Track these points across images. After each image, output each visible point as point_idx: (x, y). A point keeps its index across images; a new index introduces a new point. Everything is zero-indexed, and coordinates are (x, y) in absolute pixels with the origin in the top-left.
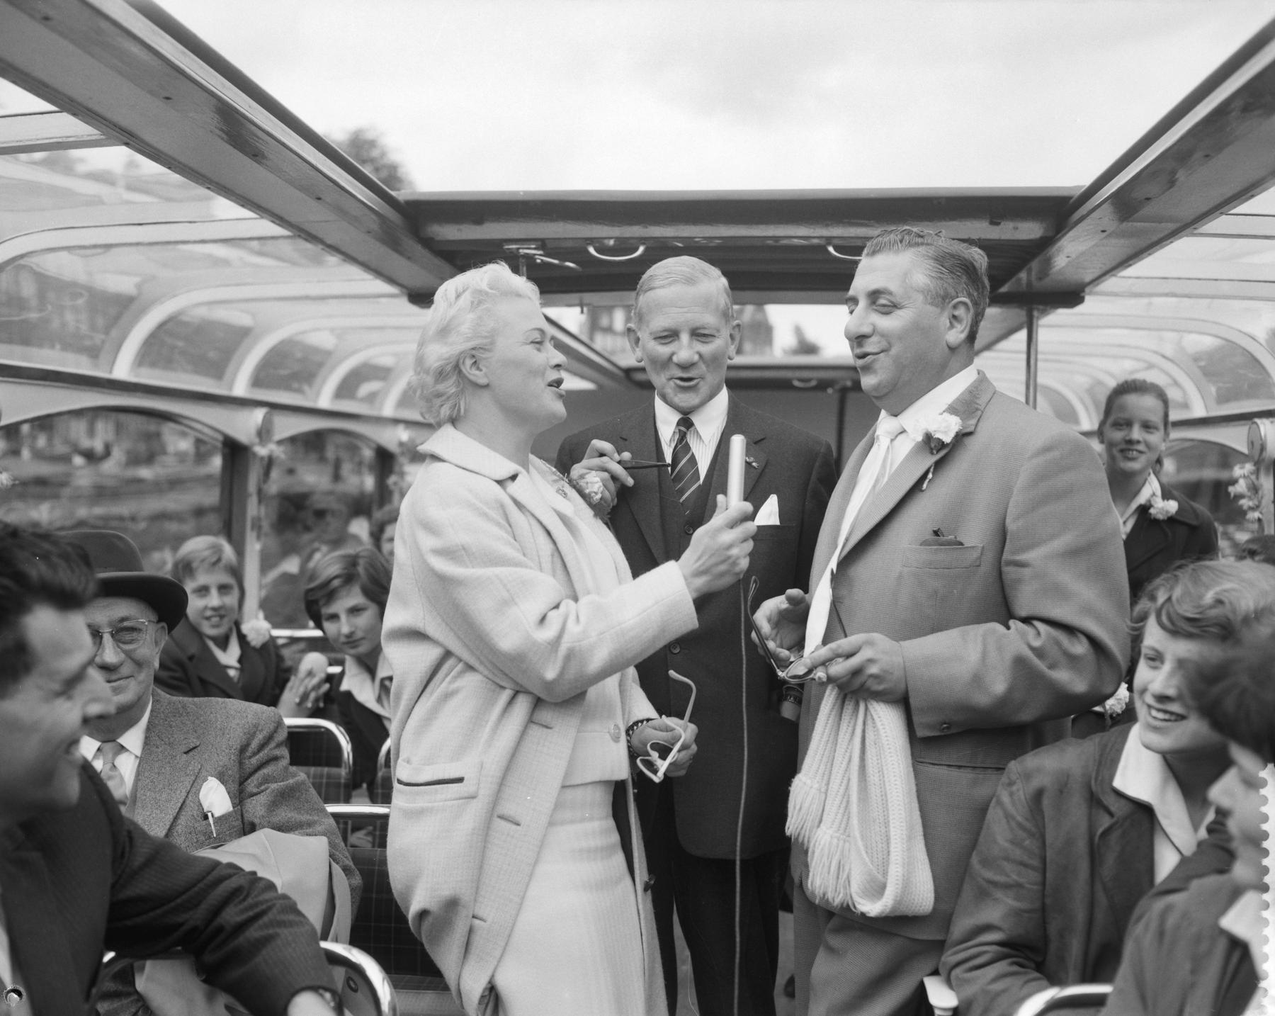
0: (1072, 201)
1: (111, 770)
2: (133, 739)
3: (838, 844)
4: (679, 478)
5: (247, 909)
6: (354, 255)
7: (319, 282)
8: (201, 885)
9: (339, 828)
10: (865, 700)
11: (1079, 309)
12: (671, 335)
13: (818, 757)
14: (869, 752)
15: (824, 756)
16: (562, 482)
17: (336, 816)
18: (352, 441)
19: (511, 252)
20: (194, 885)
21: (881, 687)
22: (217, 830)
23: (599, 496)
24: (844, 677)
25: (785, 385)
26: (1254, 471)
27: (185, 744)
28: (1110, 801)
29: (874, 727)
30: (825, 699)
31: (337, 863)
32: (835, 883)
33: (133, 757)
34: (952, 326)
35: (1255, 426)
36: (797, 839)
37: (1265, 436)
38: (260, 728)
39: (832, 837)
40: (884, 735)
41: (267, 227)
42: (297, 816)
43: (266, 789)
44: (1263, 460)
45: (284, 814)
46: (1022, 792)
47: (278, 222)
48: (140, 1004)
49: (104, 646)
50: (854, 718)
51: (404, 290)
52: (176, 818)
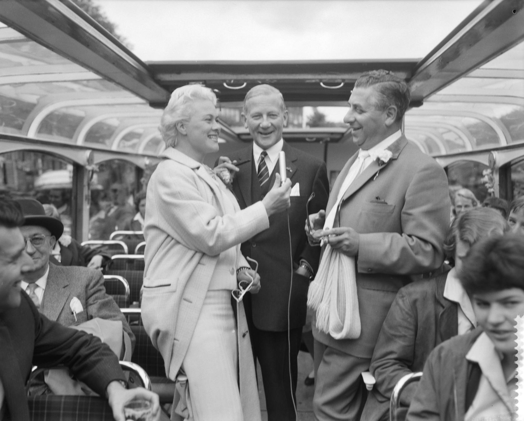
2: (42, 282)
4: (261, 176)
5: (90, 349)
8: (71, 339)
11: (421, 108)
12: (259, 115)
17: (125, 313)
20: (68, 339)
25: (303, 140)
34: (388, 116)
37: (496, 158)
38: (94, 278)
41: (92, 75)
43: (97, 302)
45: (104, 312)
48: (46, 388)
49: (27, 246)
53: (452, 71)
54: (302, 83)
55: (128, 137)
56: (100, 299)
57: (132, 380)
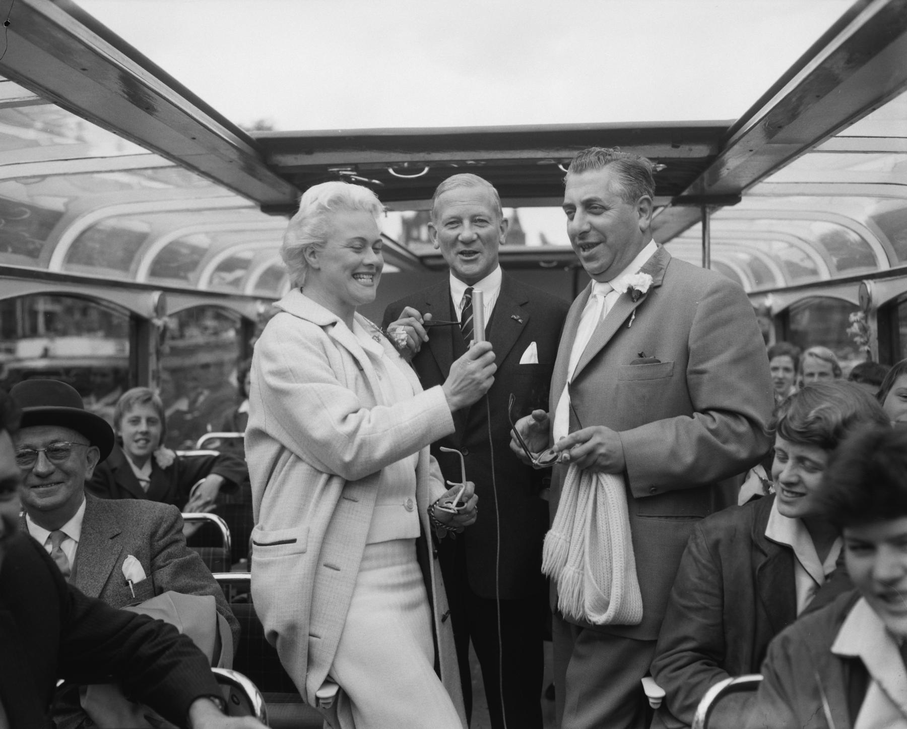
0: (729, 129)
1: (58, 551)
2: (72, 528)
3: (578, 577)
6: (221, 178)
7: (196, 198)
9: (223, 591)
10: (597, 473)
11: (738, 206)
12: (456, 222)
13: (564, 517)
14: (599, 510)
15: (570, 512)
16: (378, 333)
17: (220, 581)
18: (220, 314)
19: (334, 174)
21: (608, 463)
22: (135, 593)
23: (404, 343)
24: (582, 456)
25: (534, 266)
26: (864, 317)
27: (111, 532)
28: (764, 546)
29: (603, 493)
30: (568, 474)
31: (223, 615)
32: (576, 605)
33: (74, 542)
34: (641, 216)
35: (863, 285)
36: (549, 576)
37: (871, 292)
38: (164, 520)
39: (574, 572)
40: (610, 497)
41: (158, 160)
42: (193, 582)
43: (170, 563)
44: (870, 309)
45: (184, 581)
46: (704, 543)
47: (165, 156)
50: (588, 487)
51: (258, 203)
52: (106, 585)
53: (790, 142)
54: (532, 164)
55: (228, 266)
56: (176, 556)
57: (235, 699)
